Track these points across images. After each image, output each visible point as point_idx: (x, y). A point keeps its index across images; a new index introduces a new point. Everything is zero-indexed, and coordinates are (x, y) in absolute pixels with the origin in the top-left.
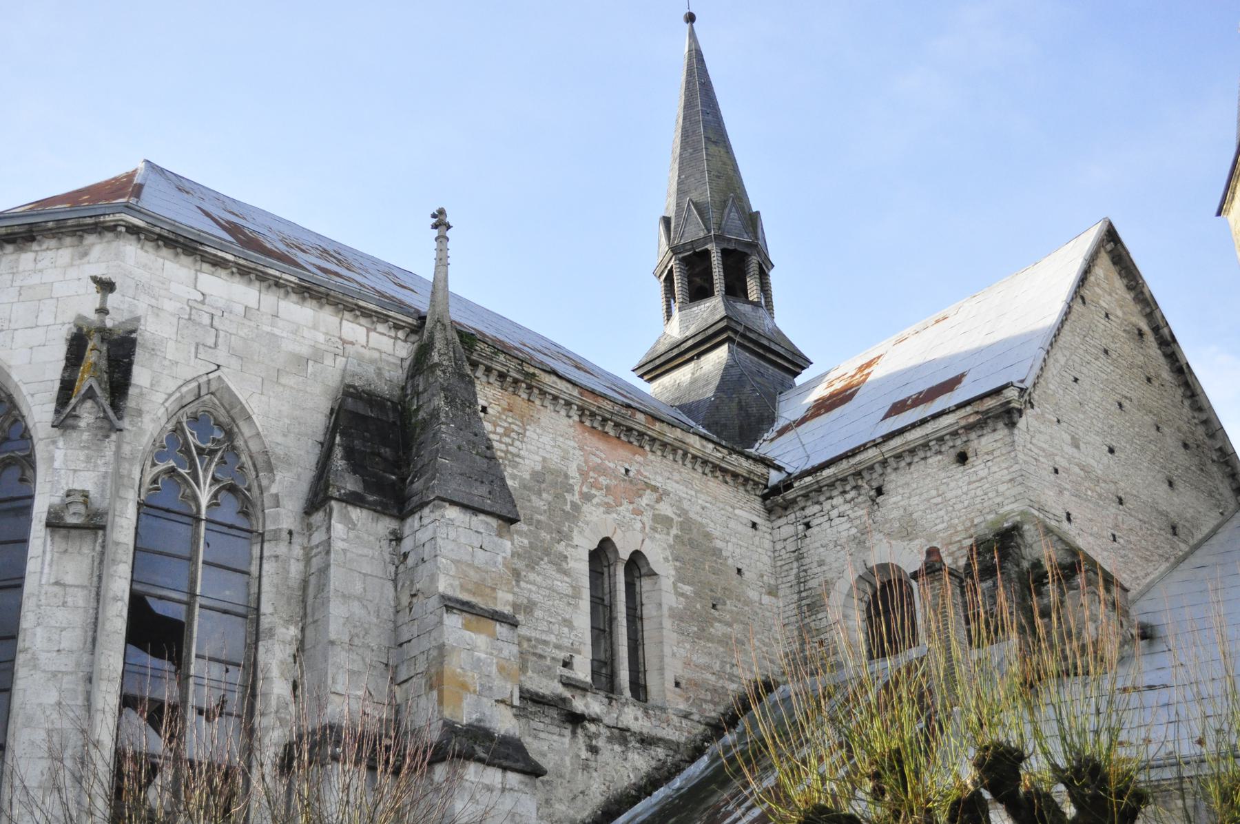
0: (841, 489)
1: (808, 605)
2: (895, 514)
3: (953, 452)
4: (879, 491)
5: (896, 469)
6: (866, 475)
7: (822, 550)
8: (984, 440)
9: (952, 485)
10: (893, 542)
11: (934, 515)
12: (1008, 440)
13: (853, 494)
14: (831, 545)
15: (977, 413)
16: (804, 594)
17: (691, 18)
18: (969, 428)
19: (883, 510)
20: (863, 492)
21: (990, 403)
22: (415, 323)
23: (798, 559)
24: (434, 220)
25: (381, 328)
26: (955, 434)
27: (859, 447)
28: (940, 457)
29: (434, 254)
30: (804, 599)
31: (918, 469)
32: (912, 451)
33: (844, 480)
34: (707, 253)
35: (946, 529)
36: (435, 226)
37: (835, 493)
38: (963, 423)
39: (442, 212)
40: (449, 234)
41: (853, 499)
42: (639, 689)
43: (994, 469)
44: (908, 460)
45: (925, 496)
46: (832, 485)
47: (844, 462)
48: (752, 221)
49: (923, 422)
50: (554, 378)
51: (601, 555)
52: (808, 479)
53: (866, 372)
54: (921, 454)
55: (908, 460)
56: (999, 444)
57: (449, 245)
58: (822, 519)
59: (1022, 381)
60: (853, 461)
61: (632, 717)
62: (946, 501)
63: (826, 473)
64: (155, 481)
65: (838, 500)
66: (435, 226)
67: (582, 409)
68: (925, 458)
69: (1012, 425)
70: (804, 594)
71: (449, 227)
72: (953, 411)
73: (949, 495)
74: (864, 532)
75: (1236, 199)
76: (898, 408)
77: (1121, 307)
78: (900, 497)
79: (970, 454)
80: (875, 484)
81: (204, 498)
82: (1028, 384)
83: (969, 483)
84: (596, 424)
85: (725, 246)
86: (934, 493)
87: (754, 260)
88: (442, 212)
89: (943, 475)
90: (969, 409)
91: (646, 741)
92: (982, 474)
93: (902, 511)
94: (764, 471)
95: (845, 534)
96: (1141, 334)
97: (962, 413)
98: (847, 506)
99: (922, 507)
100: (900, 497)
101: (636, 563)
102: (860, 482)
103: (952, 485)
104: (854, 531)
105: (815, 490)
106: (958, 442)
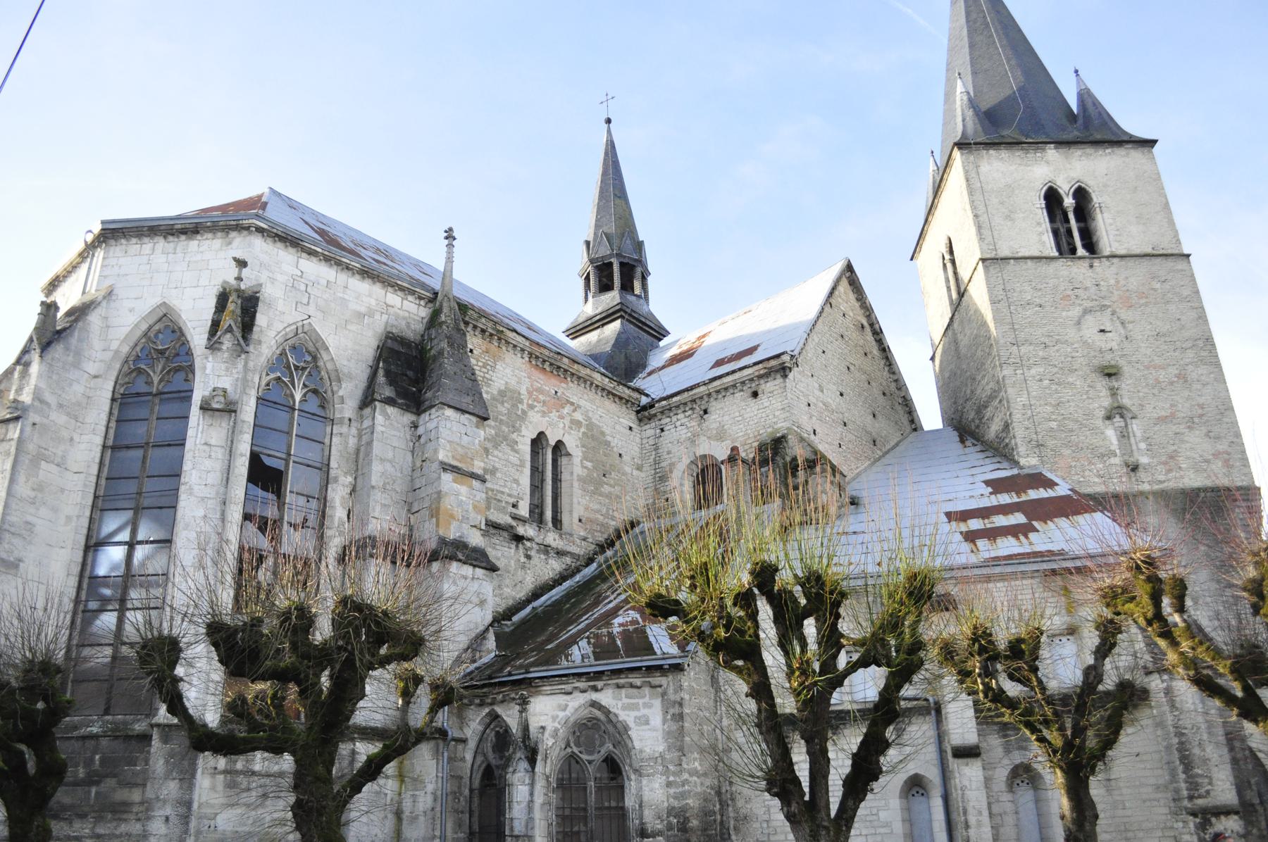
2: (715, 426)
3: (750, 391)
4: (706, 412)
17: (609, 121)
18: (760, 377)
21: (773, 363)
25: (410, 298)
26: (752, 380)
31: (729, 400)
34: (611, 264)
36: (446, 238)
39: (451, 229)
42: (557, 522)
46: (678, 407)
48: (639, 246)
49: (734, 372)
51: (538, 442)
61: (552, 538)
63: (675, 399)
64: (268, 385)
65: (681, 416)
66: (446, 238)
67: (531, 354)
76: (719, 363)
81: (298, 397)
82: (796, 353)
87: (639, 270)
88: (451, 229)
91: (560, 553)
96: (863, 327)
101: (559, 447)
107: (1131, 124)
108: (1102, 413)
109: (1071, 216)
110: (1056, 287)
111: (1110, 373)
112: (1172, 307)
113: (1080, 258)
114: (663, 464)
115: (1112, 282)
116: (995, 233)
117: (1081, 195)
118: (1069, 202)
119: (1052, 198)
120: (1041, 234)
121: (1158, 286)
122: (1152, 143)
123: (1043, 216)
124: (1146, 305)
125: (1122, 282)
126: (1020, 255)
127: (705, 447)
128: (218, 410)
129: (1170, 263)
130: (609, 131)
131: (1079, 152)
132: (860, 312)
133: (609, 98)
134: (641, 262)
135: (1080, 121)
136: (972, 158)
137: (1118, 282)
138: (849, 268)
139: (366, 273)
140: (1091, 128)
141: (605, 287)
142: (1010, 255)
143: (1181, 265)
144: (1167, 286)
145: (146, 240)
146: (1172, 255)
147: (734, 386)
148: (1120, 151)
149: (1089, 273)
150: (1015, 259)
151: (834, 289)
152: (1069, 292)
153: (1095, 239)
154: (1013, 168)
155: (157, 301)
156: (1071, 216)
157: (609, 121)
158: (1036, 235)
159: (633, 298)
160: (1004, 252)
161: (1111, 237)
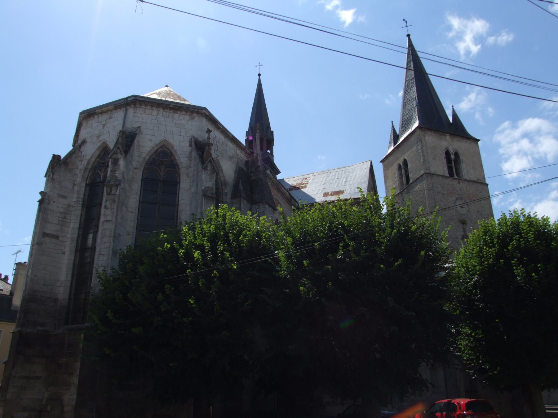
17: (259, 75)
108: (460, 237)
109: (453, 162)
111: (463, 223)
113: (456, 179)
117: (456, 154)
118: (453, 157)
119: (447, 153)
120: (444, 167)
121: (478, 194)
123: (444, 161)
128: (210, 197)
131: (456, 139)
139: (102, 113)
145: (154, 108)
148: (469, 142)
155: (162, 138)
156: (453, 162)
157: (259, 75)
158: (441, 168)
160: (432, 171)
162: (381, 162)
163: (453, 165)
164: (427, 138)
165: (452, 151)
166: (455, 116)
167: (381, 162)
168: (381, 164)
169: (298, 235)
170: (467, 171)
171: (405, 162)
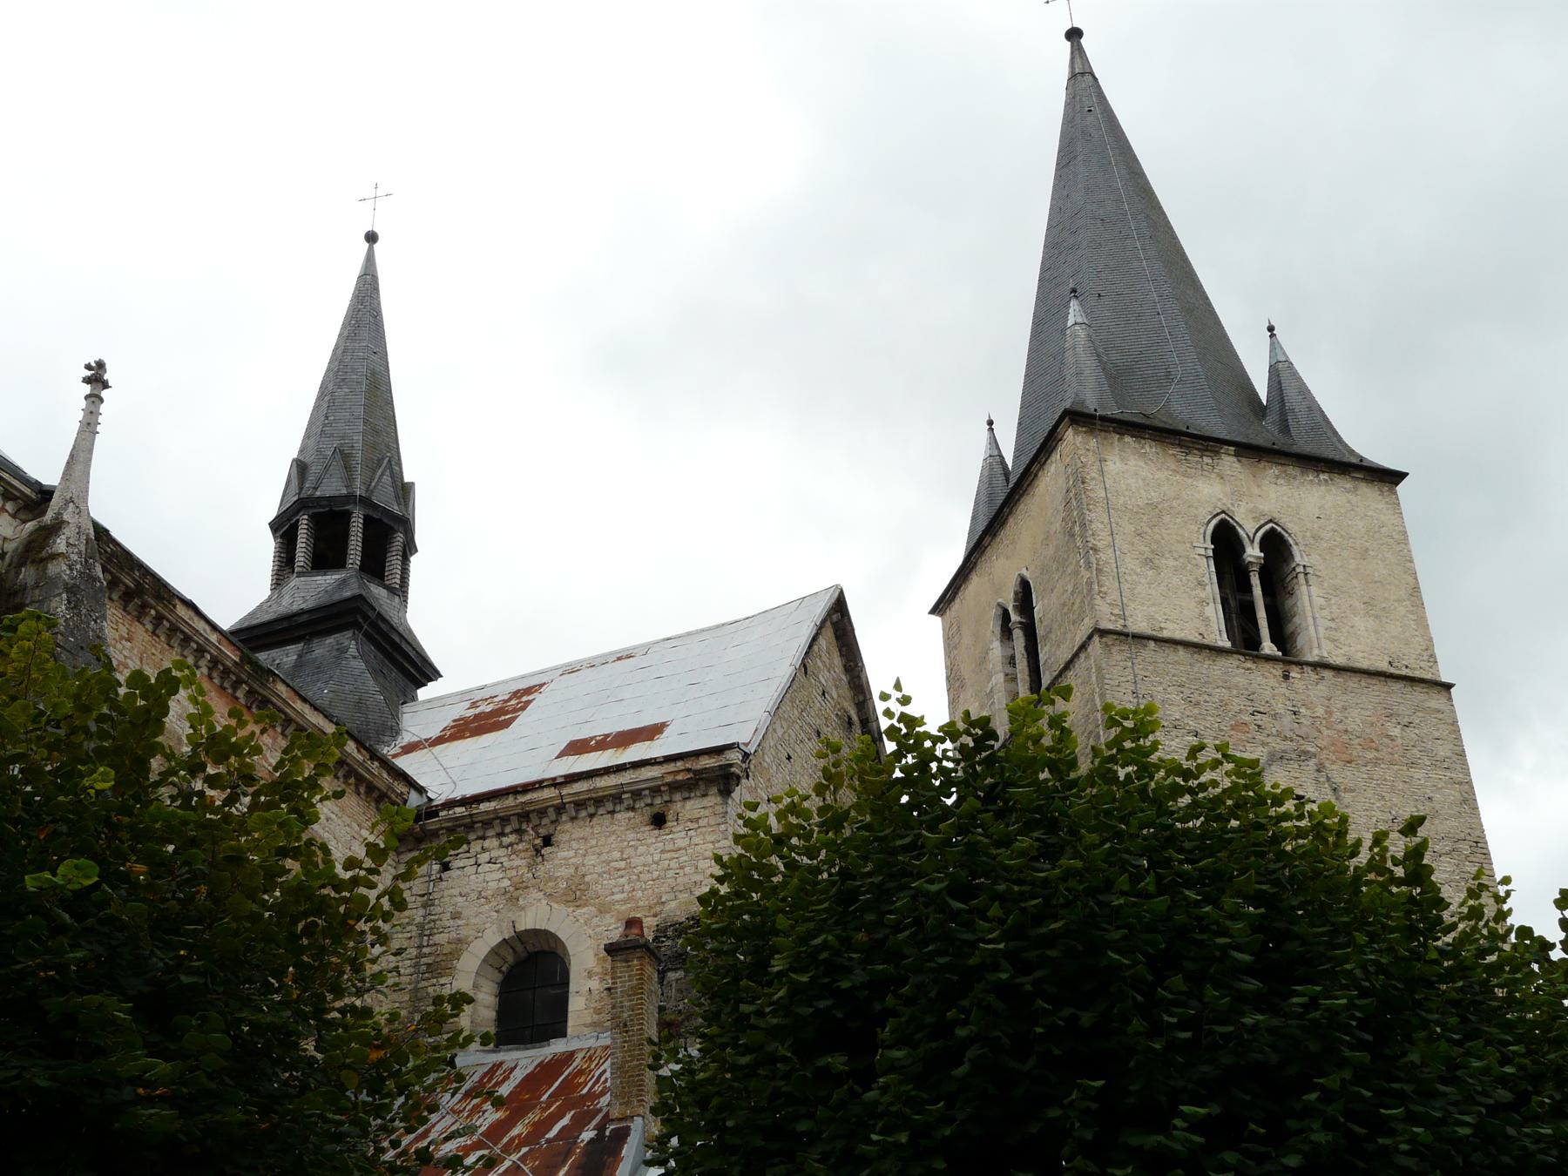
0: (498, 829)
1: (428, 965)
2: (564, 872)
3: (648, 811)
4: (547, 841)
5: (573, 819)
6: (535, 820)
7: (460, 899)
8: (689, 804)
9: (641, 849)
10: (555, 905)
11: (613, 882)
12: (719, 809)
13: (512, 838)
14: (474, 896)
15: (689, 770)
16: (426, 950)
17: (371, 238)
18: (675, 787)
19: (548, 865)
20: (526, 838)
21: (707, 762)
22: (33, 496)
23: (424, 906)
24: (89, 373)
26: (656, 791)
27: (534, 783)
28: (631, 814)
29: (80, 415)
30: (425, 956)
31: (601, 824)
32: (599, 802)
33: (505, 820)
34: (348, 514)
35: (625, 901)
36: (87, 380)
37: (490, 833)
38: (669, 779)
39: (101, 365)
40: (104, 394)
41: (511, 845)
43: (696, 840)
44: (591, 810)
45: (604, 857)
46: (487, 824)
47: (511, 798)
48: (405, 492)
49: (620, 768)
50: (191, 613)
52: (460, 810)
53: (525, 699)
54: (610, 806)
55: (591, 810)
56: (707, 812)
57: (103, 408)
58: (467, 862)
59: (746, 745)
60: (521, 799)
62: (630, 867)
63: (484, 807)
65: (491, 843)
66: (87, 380)
68: (612, 812)
69: (726, 793)
70: (426, 950)
71: (106, 385)
72: (660, 763)
73: (635, 861)
74: (520, 886)
75: (957, 601)
76: (578, 747)
77: (837, 687)
78: (572, 853)
79: (670, 817)
80: (543, 831)
82: (751, 749)
83: (663, 852)
84: (226, 684)
85: (370, 513)
86: (617, 855)
87: (400, 538)
88: (101, 365)
89: (631, 835)
90: (680, 765)
92: (680, 843)
93: (572, 871)
94: (405, 790)
95: (493, 885)
96: (850, 723)
97: (671, 767)
98: (502, 852)
99: (599, 869)
100: (572, 853)
102: (524, 826)
103: (641, 849)
104: (506, 883)
105: (465, 826)
106: (658, 801)
107: (1363, 437)
109: (1255, 580)
110: (1223, 704)
112: (1418, 774)
113: (1269, 659)
114: (438, 938)
115: (1320, 711)
116: (1125, 587)
117: (1275, 544)
118: (1253, 553)
119: (1225, 539)
121: (1396, 732)
122: (1392, 478)
123: (1208, 570)
124: (1376, 762)
125: (1337, 715)
126: (1165, 634)
127: (536, 915)
129: (1418, 695)
130: (370, 259)
131: (1274, 471)
132: (846, 691)
133: (377, 195)
134: (405, 524)
135: (1272, 417)
136: (1093, 443)
137: (1329, 713)
138: (839, 608)
140: (1284, 434)
141: (327, 557)
142: (1149, 632)
143: (1435, 701)
144: (1411, 733)
146: (1422, 681)
147: (617, 798)
148: (1345, 483)
149: (1282, 689)
150: (1157, 640)
151: (814, 639)
152: (1247, 718)
153: (1290, 628)
154: (1161, 475)
156: (1255, 580)
157: (371, 238)
159: (383, 592)
160: (1139, 625)
161: (1321, 630)
162: (934, 611)
163: (1257, 591)
164: (1114, 465)
165: (1249, 527)
166: (1280, 372)
167: (934, 611)
168: (937, 621)
169: (606, 1040)
170: (1325, 615)
171: (1025, 594)
